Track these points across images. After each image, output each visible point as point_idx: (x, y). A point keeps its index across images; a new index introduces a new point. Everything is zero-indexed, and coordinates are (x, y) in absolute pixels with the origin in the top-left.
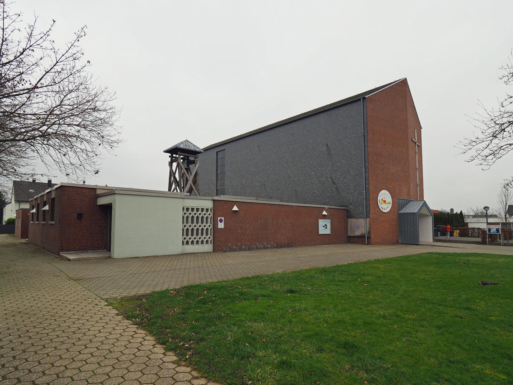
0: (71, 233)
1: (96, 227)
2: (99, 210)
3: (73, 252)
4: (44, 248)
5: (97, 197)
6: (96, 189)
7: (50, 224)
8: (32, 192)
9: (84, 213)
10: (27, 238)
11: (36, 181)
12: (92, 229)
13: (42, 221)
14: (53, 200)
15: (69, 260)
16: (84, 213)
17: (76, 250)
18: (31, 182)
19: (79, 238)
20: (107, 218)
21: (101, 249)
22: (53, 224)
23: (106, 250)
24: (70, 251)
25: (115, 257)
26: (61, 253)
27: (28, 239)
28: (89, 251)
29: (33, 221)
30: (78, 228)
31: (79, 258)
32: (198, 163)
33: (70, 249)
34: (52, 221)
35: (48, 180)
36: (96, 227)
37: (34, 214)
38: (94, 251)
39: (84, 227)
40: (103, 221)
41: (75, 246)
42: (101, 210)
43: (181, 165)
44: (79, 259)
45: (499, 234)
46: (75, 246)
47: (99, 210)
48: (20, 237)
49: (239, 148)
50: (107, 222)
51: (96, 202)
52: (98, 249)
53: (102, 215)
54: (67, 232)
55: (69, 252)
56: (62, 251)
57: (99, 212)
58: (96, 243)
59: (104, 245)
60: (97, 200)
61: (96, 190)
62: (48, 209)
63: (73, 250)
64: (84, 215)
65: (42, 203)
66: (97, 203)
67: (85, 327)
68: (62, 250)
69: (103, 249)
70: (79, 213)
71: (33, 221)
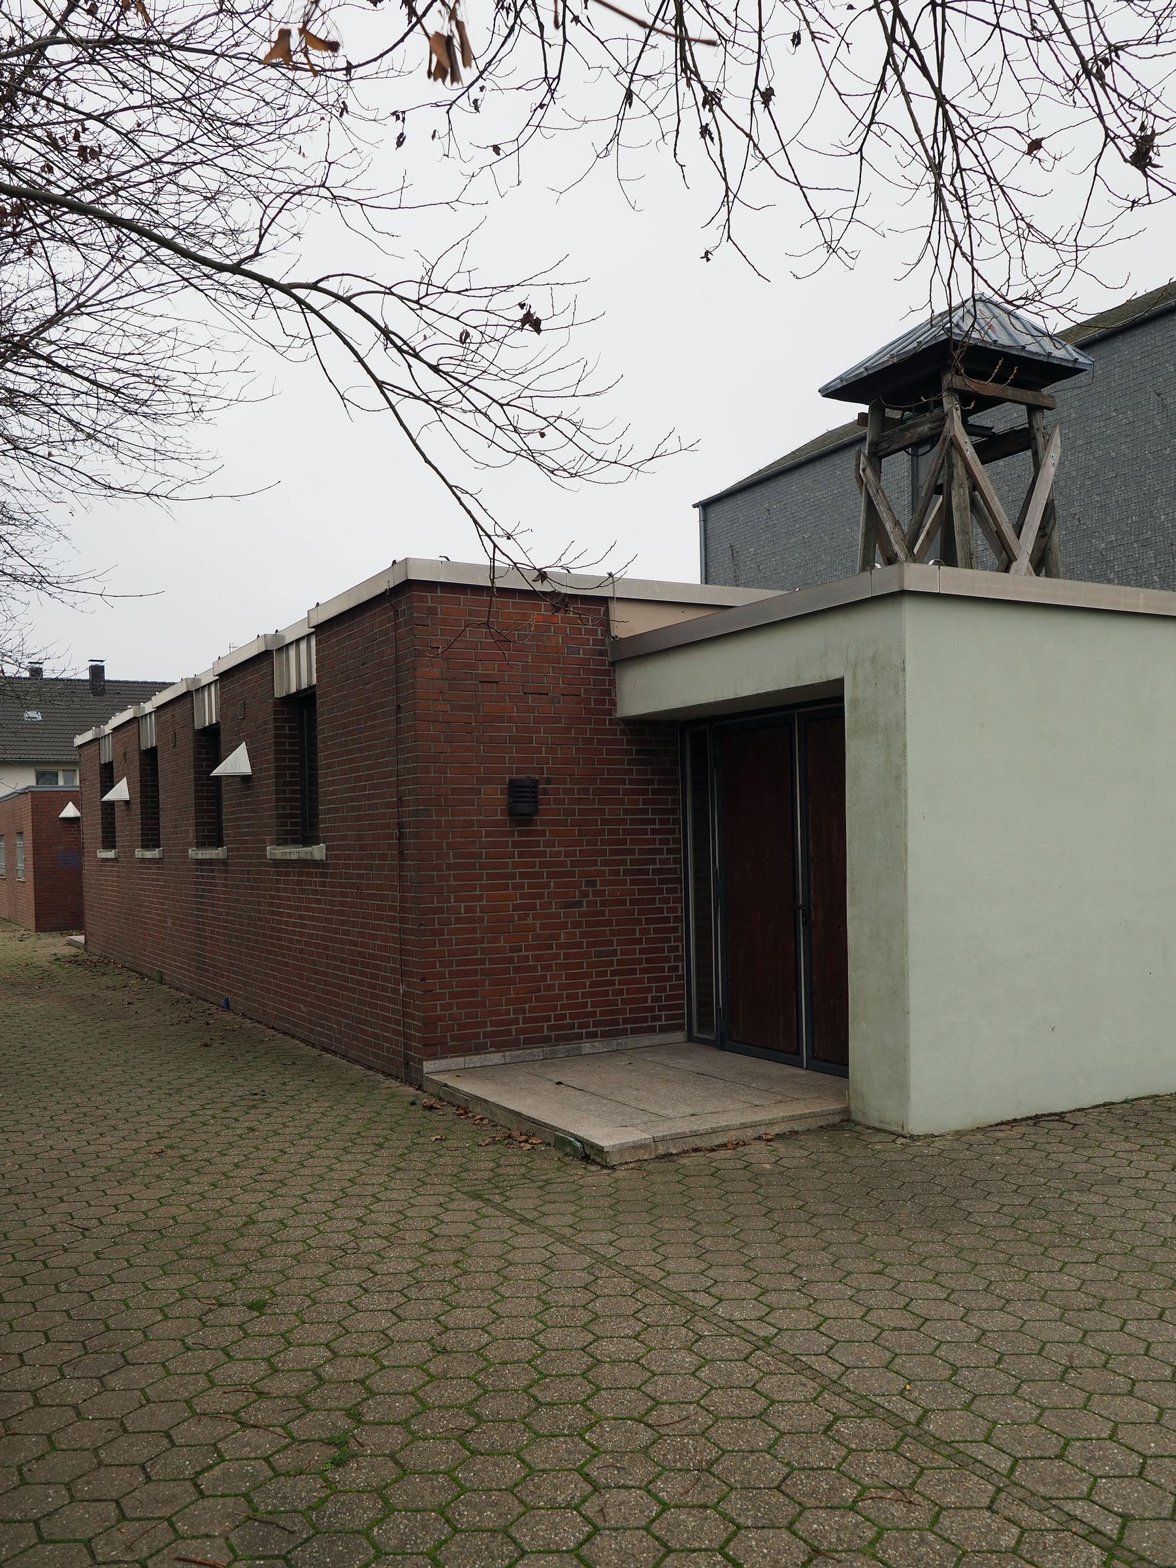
0: (481, 920)
1: (616, 873)
2: (629, 752)
3: (495, 1058)
4: (227, 1006)
5: (613, 664)
6: (604, 601)
7: (277, 863)
8: (33, 723)
9: (548, 781)
10: (79, 927)
11: (47, 675)
12: (596, 893)
13: (190, 845)
14: (283, 713)
15: (589, 1154)
16: (548, 781)
17: (514, 1044)
18: (25, 678)
19: (526, 958)
20: (674, 812)
21: (651, 1030)
22: (316, 864)
23: (679, 1036)
24: (479, 1049)
25: (916, 1126)
26: (428, 1066)
27: (81, 939)
28: (587, 1047)
29: (109, 843)
30: (516, 887)
31: (663, 1139)
32: (1056, 440)
33: (477, 1036)
34: (307, 841)
35: (91, 667)
36: (616, 873)
37: (119, 812)
38: (614, 1043)
39: (550, 875)
40: (654, 832)
41: (507, 1012)
42: (639, 752)
43: (968, 454)
44: (661, 1150)
45: (514, 836)
46: (507, 1012)
47: (629, 752)
48: (31, 923)
49: (1076, 404)
50: (676, 841)
51: (607, 694)
52: (634, 1032)
53: (645, 792)
54: (458, 921)
55: (476, 1060)
56: (433, 1056)
57: (630, 772)
58: (620, 992)
59: (668, 998)
60: (613, 683)
61: (607, 610)
62: (245, 768)
63: (500, 1047)
64: (545, 792)
65: (187, 743)
66: (613, 703)
67: (200, 1156)
68: (437, 1048)
69: (664, 1029)
70: (514, 776)
71: (114, 847)
